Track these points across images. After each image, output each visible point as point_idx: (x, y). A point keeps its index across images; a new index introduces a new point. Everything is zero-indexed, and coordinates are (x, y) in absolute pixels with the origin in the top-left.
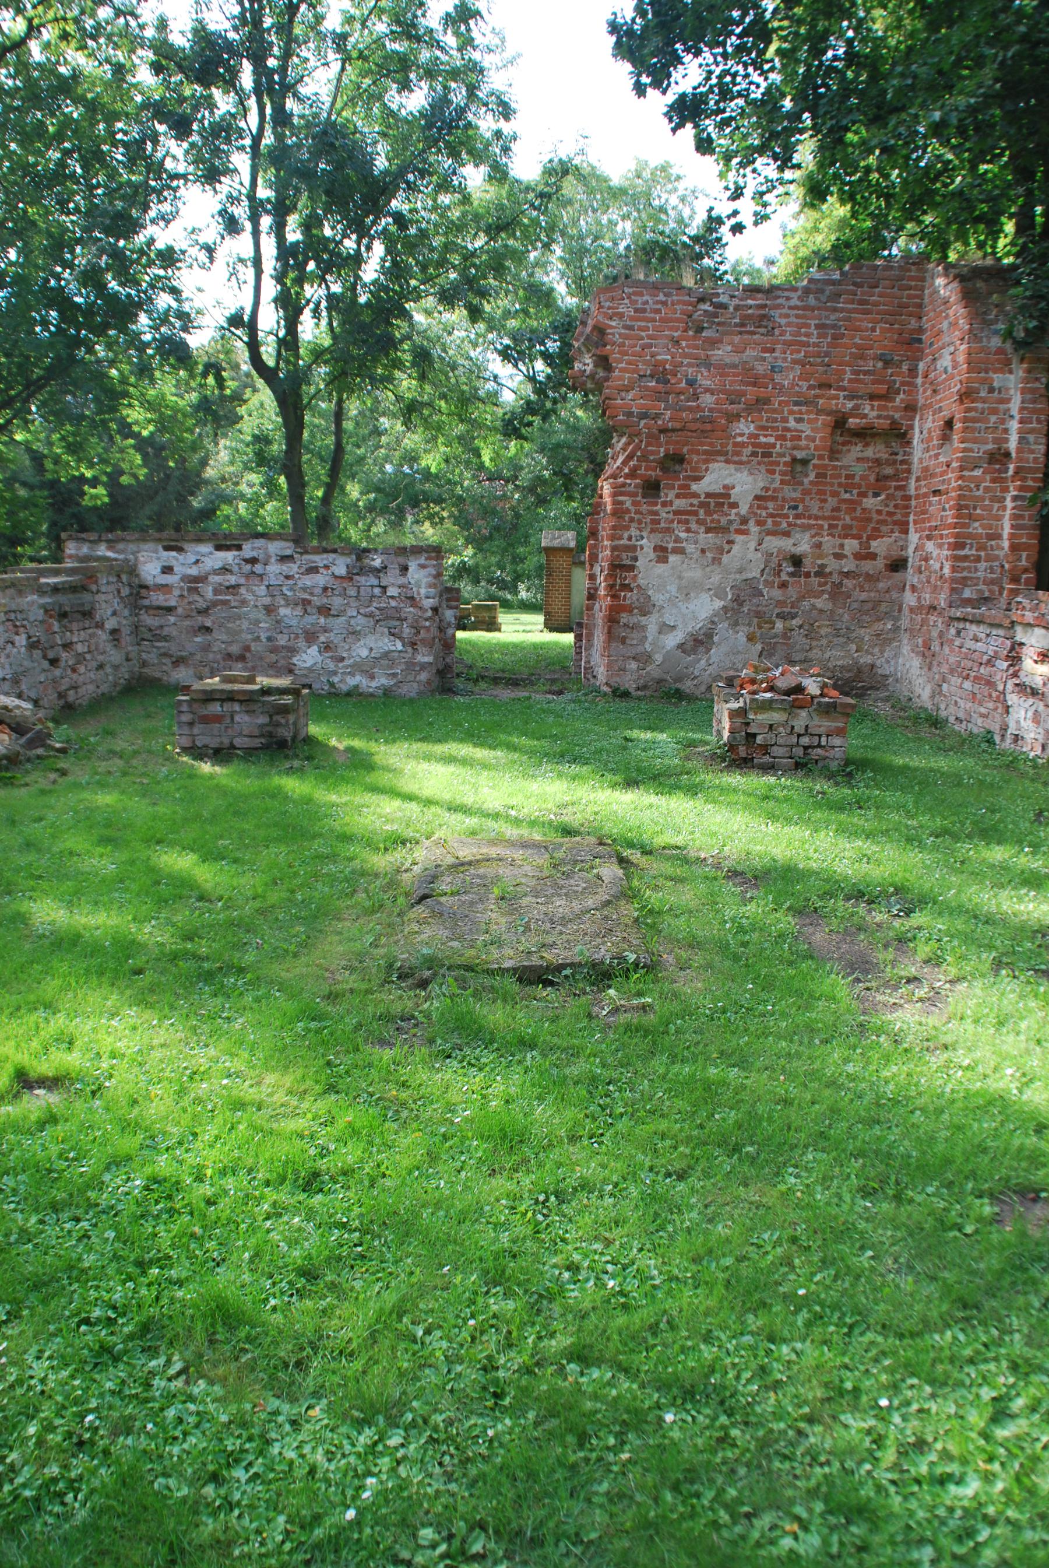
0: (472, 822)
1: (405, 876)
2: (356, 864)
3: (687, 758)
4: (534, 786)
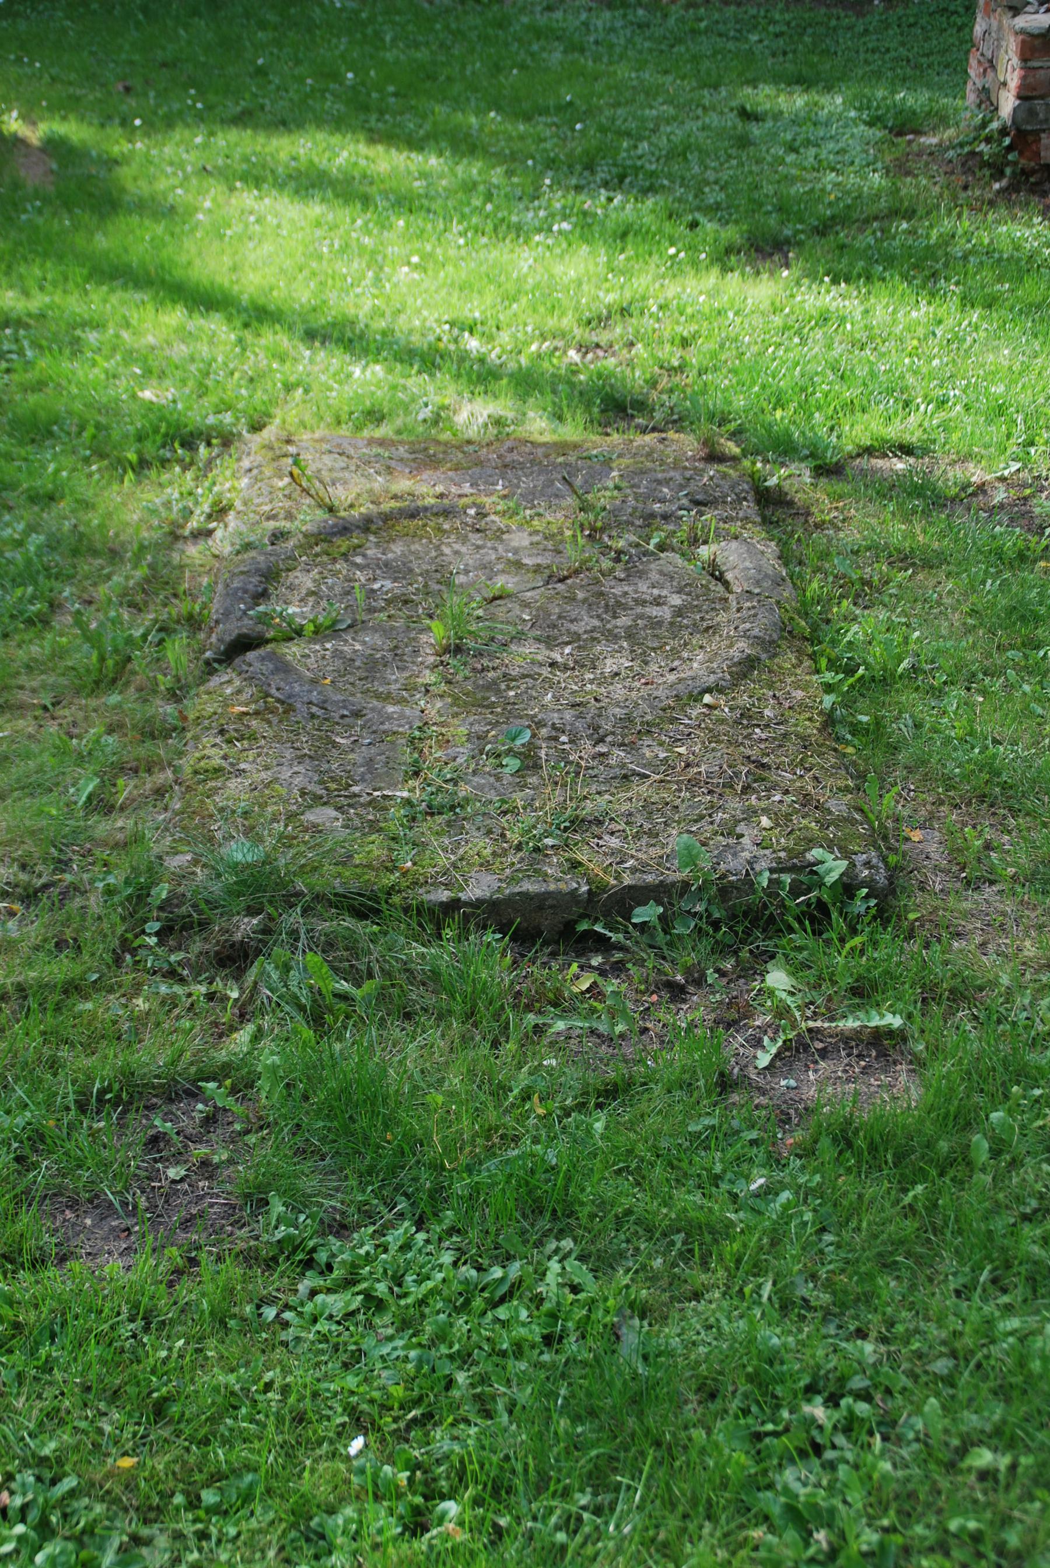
0: (368, 377)
1: (193, 551)
2: (61, 518)
3: (901, 168)
4: (523, 260)
